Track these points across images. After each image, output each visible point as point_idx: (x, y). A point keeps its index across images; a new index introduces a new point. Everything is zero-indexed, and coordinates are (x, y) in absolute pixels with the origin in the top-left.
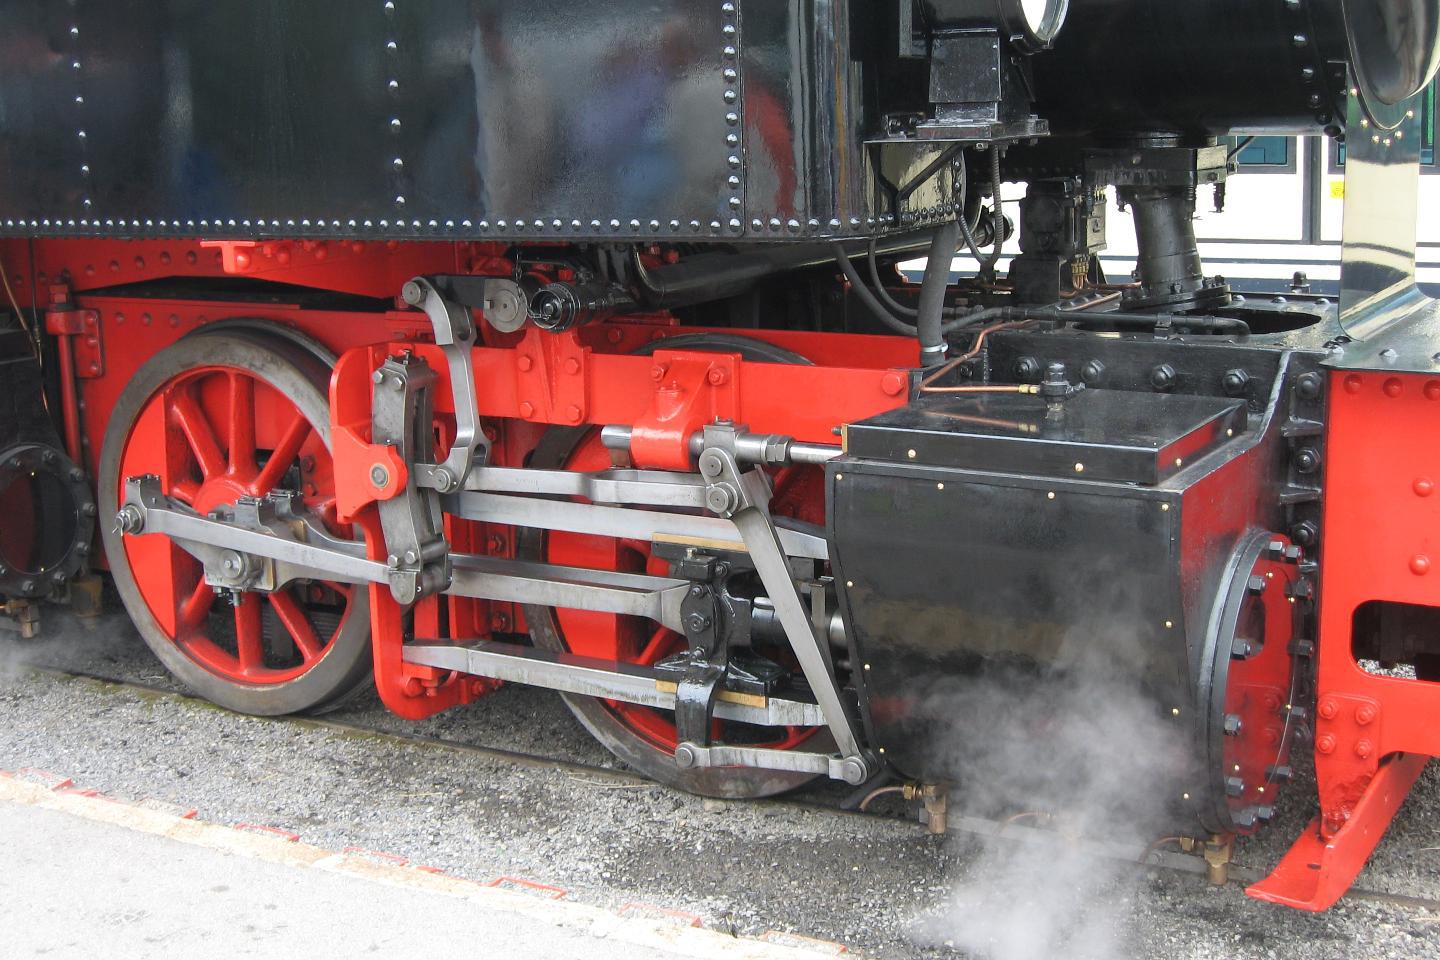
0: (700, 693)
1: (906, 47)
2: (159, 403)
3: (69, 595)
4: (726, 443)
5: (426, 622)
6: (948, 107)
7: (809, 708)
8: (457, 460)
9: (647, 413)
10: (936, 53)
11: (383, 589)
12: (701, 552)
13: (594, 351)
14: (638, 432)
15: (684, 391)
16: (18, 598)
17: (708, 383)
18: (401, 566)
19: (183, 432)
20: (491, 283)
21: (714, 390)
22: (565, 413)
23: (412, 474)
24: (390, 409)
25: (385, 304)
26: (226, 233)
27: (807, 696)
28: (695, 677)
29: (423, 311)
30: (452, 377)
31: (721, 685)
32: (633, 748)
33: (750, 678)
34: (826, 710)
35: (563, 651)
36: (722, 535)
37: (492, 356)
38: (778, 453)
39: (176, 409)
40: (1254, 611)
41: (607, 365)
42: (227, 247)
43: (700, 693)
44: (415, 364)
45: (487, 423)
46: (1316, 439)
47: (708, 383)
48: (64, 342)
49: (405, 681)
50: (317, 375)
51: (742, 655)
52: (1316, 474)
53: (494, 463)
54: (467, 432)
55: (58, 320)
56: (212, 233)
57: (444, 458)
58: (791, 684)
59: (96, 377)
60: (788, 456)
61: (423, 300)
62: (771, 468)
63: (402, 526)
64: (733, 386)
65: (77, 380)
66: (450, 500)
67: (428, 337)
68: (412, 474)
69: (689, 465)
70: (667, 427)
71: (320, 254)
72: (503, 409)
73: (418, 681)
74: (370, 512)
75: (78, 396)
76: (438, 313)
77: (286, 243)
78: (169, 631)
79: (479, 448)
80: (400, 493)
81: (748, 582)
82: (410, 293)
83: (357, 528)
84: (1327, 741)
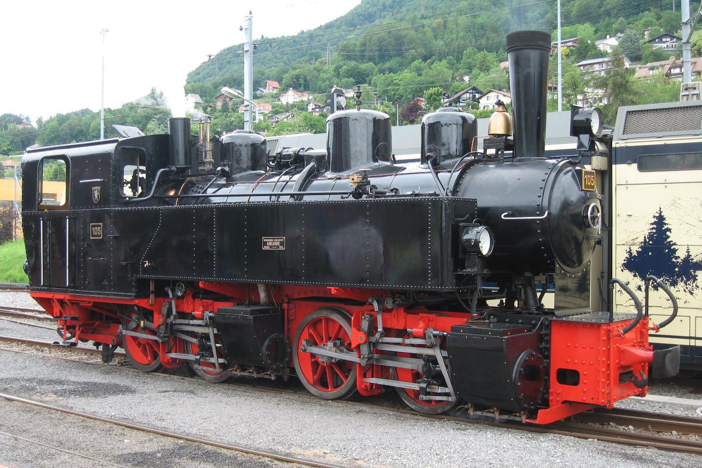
0: (424, 385)
1: (460, 256)
2: (307, 328)
3: (281, 373)
4: (432, 332)
5: (369, 373)
6: (469, 267)
7: (447, 389)
8: (377, 335)
9: (416, 326)
10: (147, 360)
11: (360, 364)
12: (425, 355)
13: (408, 314)
14: (414, 330)
15: (424, 322)
16: (272, 370)
17: (429, 320)
18: (363, 358)
19: (312, 334)
20: (386, 298)
21: (430, 322)
22: (401, 327)
23: (368, 339)
24: (365, 325)
25: (362, 304)
26: (332, 286)
27: (445, 385)
28: (424, 382)
29: (373, 305)
30: (75, 155)
31: (429, 384)
32: (419, 407)
33: (435, 382)
34: (449, 389)
35: (397, 378)
36: (430, 352)
37: (387, 315)
38: (441, 333)
39: (310, 330)
40: (526, 365)
41: (410, 316)
42: (332, 288)
43: (424, 385)
44: (371, 316)
45: (384, 328)
46: (549, 335)
47: (429, 320)
48: (286, 311)
49: (363, 386)
50: (348, 320)
51: (434, 378)
52: (549, 342)
53: (386, 336)
54: (380, 329)
55: (285, 305)
56: (329, 285)
57: (375, 335)
58: (444, 384)
59: (293, 320)
60: (443, 334)
61: (372, 302)
62: (440, 337)
63: (365, 350)
64: (434, 321)
65: (288, 320)
66: (375, 344)
67: (373, 310)
68: (368, 339)
69: (423, 337)
70: (420, 328)
71: (351, 291)
72: (388, 326)
73: (366, 386)
74: (358, 347)
75: (288, 324)
76: (375, 305)
77: (344, 288)
78: (310, 381)
79: (382, 333)
80: (365, 343)
81: (435, 362)
82: (370, 300)
83: (354, 350)
84: (551, 398)
